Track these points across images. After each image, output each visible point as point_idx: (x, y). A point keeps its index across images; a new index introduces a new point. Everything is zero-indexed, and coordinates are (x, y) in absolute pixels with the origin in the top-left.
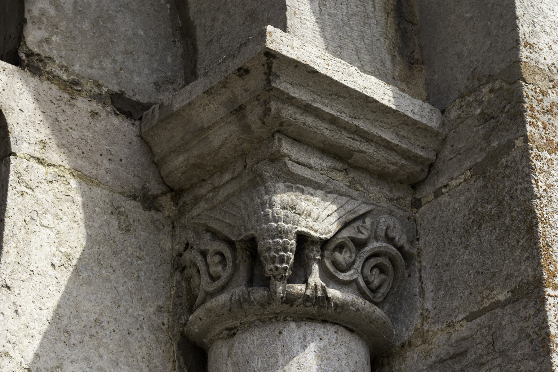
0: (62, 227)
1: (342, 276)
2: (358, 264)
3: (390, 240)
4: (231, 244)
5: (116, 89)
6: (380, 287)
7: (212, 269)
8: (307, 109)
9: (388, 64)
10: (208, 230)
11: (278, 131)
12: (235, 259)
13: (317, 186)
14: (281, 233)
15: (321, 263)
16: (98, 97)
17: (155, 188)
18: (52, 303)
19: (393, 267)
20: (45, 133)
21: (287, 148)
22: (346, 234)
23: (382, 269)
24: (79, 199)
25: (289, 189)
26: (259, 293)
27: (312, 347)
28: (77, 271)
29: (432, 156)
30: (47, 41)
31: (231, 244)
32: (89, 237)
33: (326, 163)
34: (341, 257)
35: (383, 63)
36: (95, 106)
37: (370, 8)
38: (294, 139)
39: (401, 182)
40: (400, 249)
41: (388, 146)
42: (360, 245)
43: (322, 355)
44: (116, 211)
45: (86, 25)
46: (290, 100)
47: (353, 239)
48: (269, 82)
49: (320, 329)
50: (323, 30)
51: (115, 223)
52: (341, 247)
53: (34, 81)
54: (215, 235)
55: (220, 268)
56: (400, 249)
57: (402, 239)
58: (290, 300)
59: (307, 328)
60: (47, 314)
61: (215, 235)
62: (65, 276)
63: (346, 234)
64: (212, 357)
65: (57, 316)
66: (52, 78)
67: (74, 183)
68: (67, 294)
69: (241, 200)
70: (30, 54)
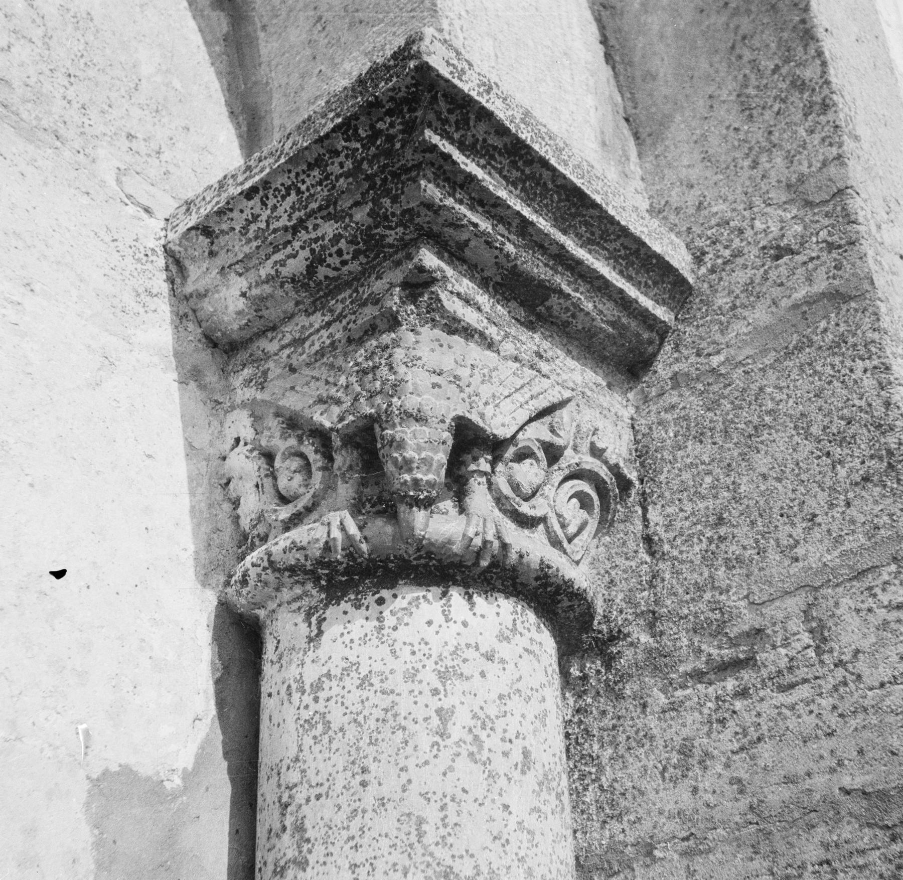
3: (596, 452)
23: (584, 501)
56: (615, 470)
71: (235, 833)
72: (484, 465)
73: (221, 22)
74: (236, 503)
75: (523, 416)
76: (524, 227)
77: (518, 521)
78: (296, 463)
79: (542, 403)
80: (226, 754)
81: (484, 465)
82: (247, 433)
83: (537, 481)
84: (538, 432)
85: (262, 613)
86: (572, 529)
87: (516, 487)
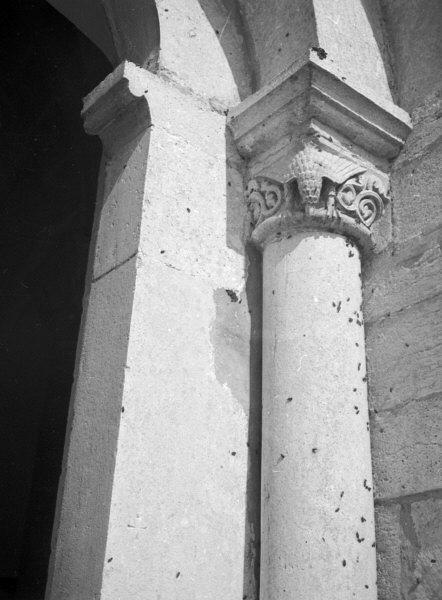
3: (376, 190)
4: (281, 187)
6: (368, 217)
7: (268, 202)
8: (332, 103)
10: (266, 179)
11: (314, 117)
12: (283, 195)
19: (347, 211)
23: (370, 207)
26: (299, 215)
31: (281, 187)
38: (322, 123)
39: (382, 157)
41: (377, 132)
46: (323, 97)
47: (355, 186)
48: (310, 84)
54: (271, 182)
55: (273, 201)
56: (381, 196)
58: (317, 219)
61: (271, 182)
64: (266, 254)
69: (226, 113)
71: (250, 434)
72: (333, 193)
73: (240, 39)
74: (253, 211)
75: (347, 176)
76: (347, 112)
77: (389, 62)
78: (272, 195)
79: (356, 172)
80: (248, 445)
81: (333, 193)
82: (256, 187)
83: (352, 199)
84: (352, 182)
85: (262, 245)
86: (366, 215)
87: (344, 199)
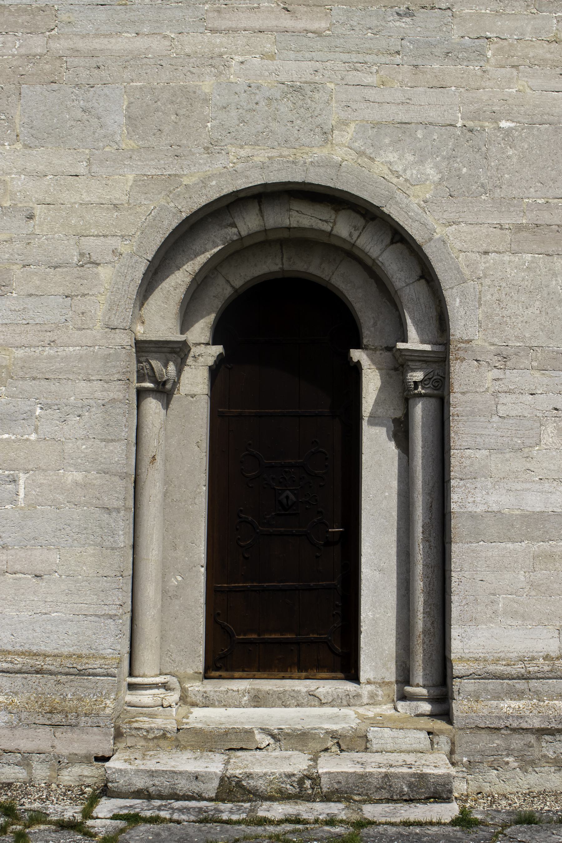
0: (375, 381)
1: (426, 386)
2: (431, 383)
5: (386, 346)
9: (436, 334)
13: (419, 369)
14: (410, 382)
15: (422, 385)
16: (382, 350)
17: (397, 366)
18: (374, 399)
20: (369, 362)
21: (409, 363)
22: (426, 378)
24: (379, 374)
25: (412, 372)
27: (421, 403)
28: (380, 390)
29: (445, 356)
30: (369, 341)
32: (382, 382)
33: (420, 363)
34: (425, 383)
35: (435, 334)
36: (381, 352)
37: (431, 321)
40: (441, 377)
42: (430, 379)
43: (422, 404)
44: (388, 374)
45: (378, 333)
49: (422, 399)
50: (418, 332)
51: (388, 377)
52: (426, 380)
53: (366, 352)
56: (441, 377)
57: (442, 375)
58: (415, 394)
59: (420, 399)
60: (373, 401)
62: (377, 392)
63: (426, 378)
65: (376, 400)
66: (371, 349)
67: (377, 371)
68: (378, 395)
70: (365, 345)
